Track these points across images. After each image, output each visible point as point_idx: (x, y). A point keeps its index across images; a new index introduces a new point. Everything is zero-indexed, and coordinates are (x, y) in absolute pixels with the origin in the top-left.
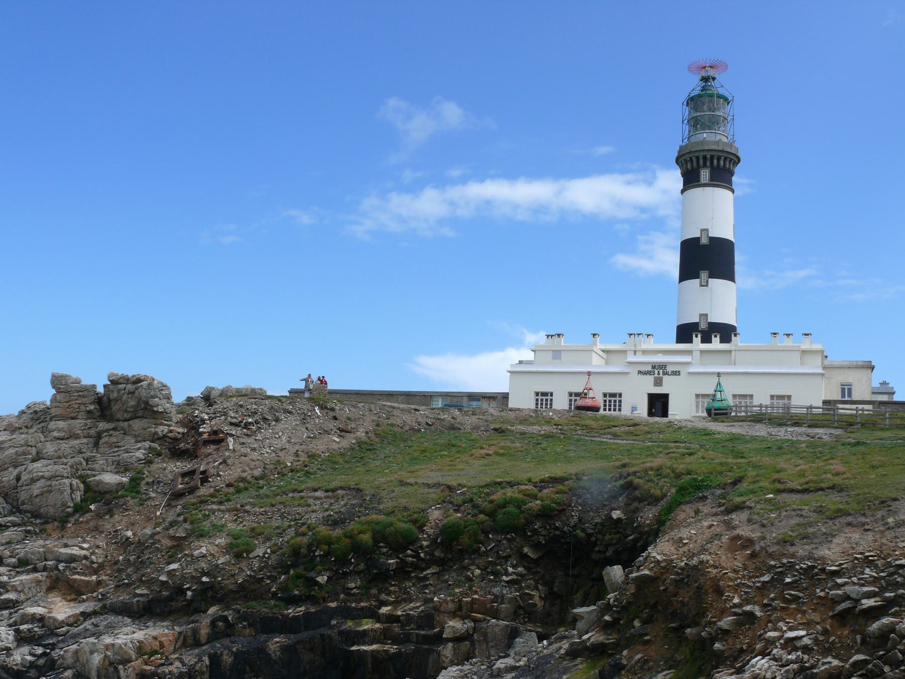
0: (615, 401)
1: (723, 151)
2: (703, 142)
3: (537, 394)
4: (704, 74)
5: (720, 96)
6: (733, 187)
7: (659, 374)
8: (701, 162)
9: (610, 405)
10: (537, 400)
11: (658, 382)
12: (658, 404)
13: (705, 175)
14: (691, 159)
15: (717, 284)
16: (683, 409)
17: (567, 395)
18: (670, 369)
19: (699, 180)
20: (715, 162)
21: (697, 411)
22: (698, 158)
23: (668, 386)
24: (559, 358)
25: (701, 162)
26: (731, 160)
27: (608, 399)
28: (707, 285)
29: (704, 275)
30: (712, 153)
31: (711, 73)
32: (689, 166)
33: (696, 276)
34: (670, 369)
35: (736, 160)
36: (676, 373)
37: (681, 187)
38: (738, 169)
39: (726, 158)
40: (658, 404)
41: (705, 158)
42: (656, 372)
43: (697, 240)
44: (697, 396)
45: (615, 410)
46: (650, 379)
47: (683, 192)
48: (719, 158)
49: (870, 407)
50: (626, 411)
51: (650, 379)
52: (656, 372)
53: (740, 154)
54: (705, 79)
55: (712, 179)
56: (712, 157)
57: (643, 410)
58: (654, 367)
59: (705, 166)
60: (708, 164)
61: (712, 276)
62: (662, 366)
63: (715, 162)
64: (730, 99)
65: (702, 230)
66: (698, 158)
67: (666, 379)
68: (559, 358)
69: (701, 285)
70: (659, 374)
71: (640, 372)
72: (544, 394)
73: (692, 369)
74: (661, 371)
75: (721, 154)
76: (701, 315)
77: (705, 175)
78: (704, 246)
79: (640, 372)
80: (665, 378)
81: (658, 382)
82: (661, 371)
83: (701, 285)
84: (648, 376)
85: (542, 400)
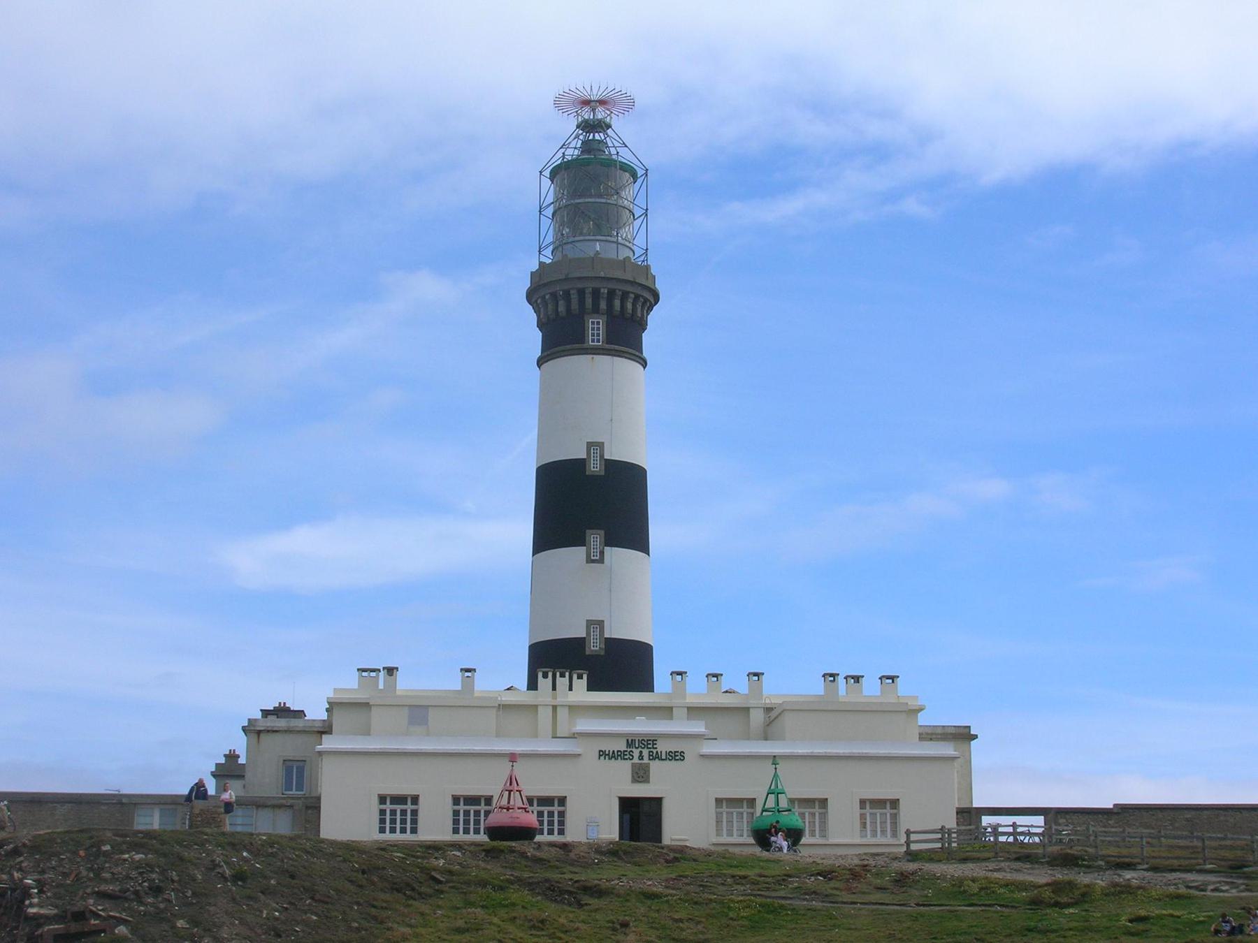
0: (404, 812)
1: (633, 283)
2: (595, 260)
3: (382, 799)
4: (587, 114)
5: (625, 168)
6: (645, 354)
7: (641, 757)
8: (589, 302)
9: (393, 821)
10: (382, 812)
11: (640, 775)
12: (640, 817)
13: (596, 328)
14: (567, 294)
15: (619, 556)
16: (687, 825)
17: (376, 800)
18: (663, 747)
19: (581, 338)
20: (617, 303)
21: (719, 832)
22: (581, 293)
23: (662, 782)
24: (423, 721)
25: (589, 302)
26: (637, 297)
27: (462, 808)
28: (601, 561)
29: (595, 538)
30: (612, 286)
31: (601, 114)
32: (562, 308)
33: (577, 540)
34: (663, 747)
35: (651, 298)
36: (676, 756)
37: (537, 352)
38: (655, 318)
39: (637, 297)
40: (640, 817)
41: (596, 293)
42: (636, 753)
43: (580, 464)
44: (719, 801)
45: (403, 831)
46: (623, 769)
47: (540, 362)
48: (625, 296)
49: (1039, 820)
50: (575, 833)
51: (623, 769)
52: (636, 753)
53: (659, 286)
54: (588, 126)
55: (609, 340)
56: (612, 293)
57: (609, 830)
58: (630, 744)
59: (596, 310)
60: (603, 305)
61: (611, 541)
62: (648, 742)
63: (617, 303)
64: (640, 172)
65: (590, 445)
66: (581, 293)
67: (657, 768)
68: (423, 721)
69: (589, 560)
70: (641, 757)
71: (602, 754)
72: (399, 799)
73: (709, 748)
74: (645, 752)
75: (629, 288)
76: (590, 623)
77: (596, 328)
78: (594, 478)
79: (602, 754)
80: (655, 766)
81: (640, 775)
82: (645, 752)
83: (589, 560)
84: (620, 762)
85: (393, 812)
